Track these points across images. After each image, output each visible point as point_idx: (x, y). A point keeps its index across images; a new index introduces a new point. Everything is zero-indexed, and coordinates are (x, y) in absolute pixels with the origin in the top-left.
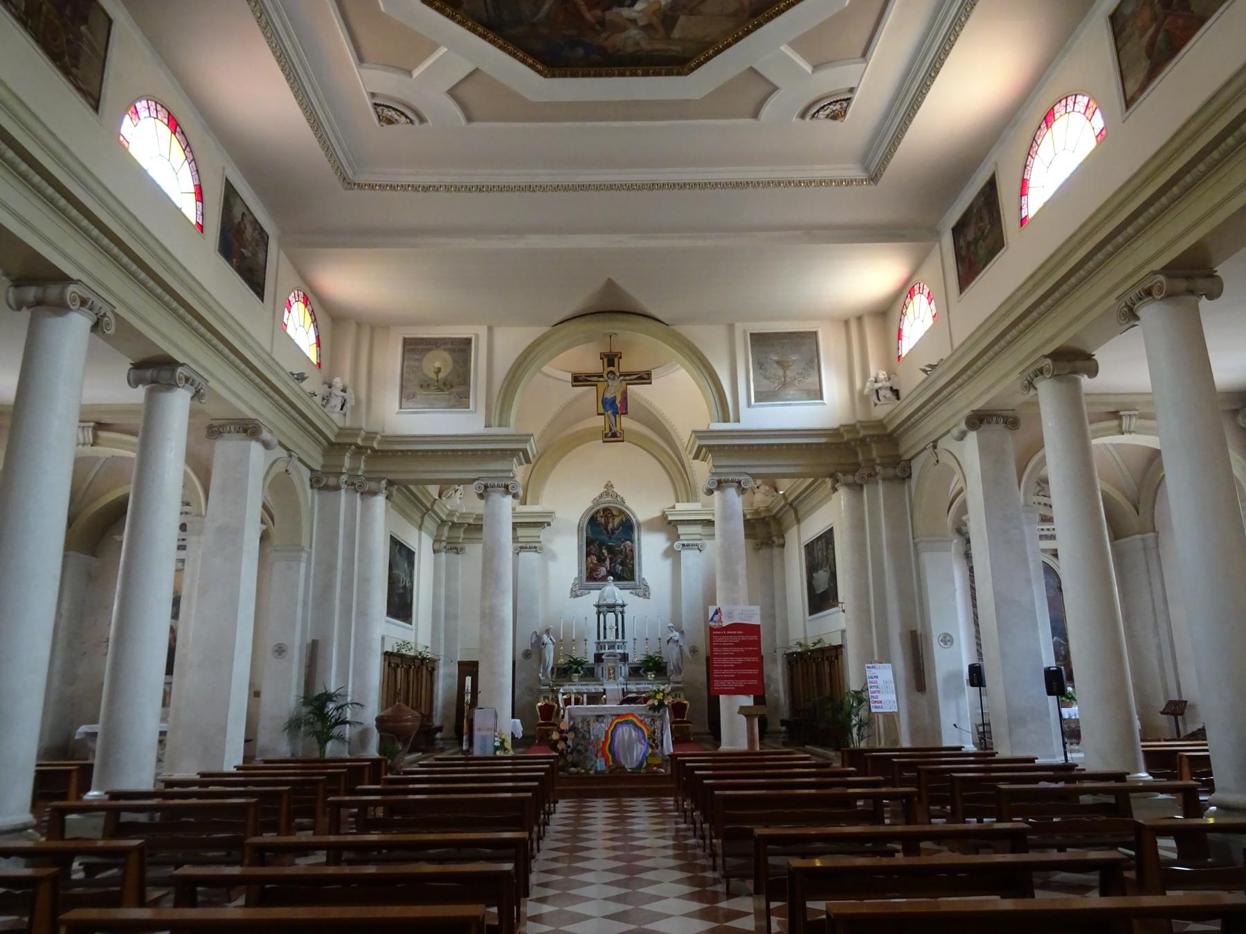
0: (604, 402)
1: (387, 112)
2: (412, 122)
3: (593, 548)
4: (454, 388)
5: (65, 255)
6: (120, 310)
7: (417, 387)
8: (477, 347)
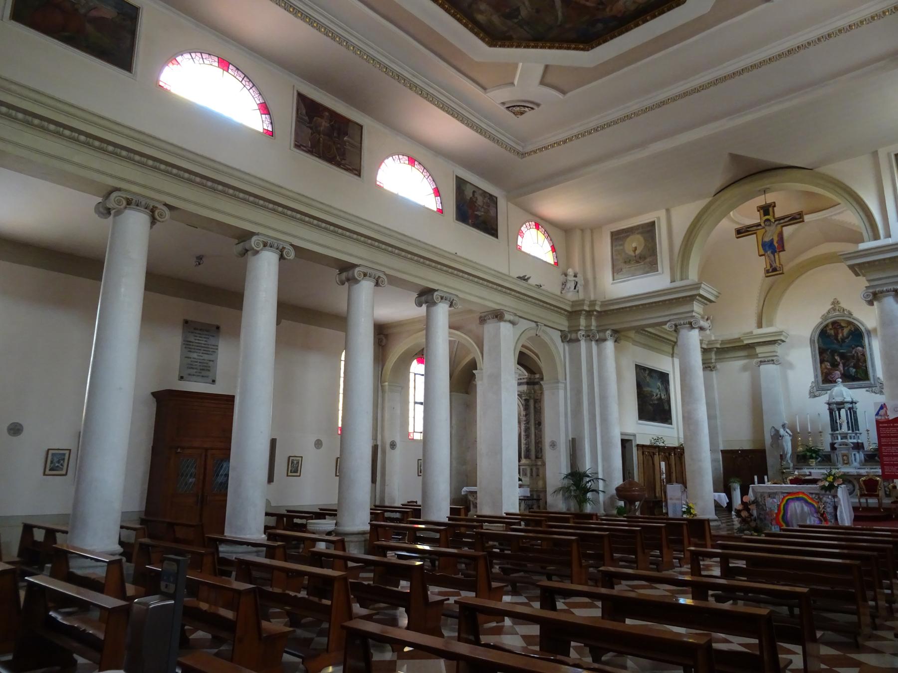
0: (764, 245)
1: (518, 108)
2: (532, 109)
3: (827, 356)
4: (646, 260)
5: (351, 255)
6: (388, 272)
7: (625, 263)
8: (659, 227)
